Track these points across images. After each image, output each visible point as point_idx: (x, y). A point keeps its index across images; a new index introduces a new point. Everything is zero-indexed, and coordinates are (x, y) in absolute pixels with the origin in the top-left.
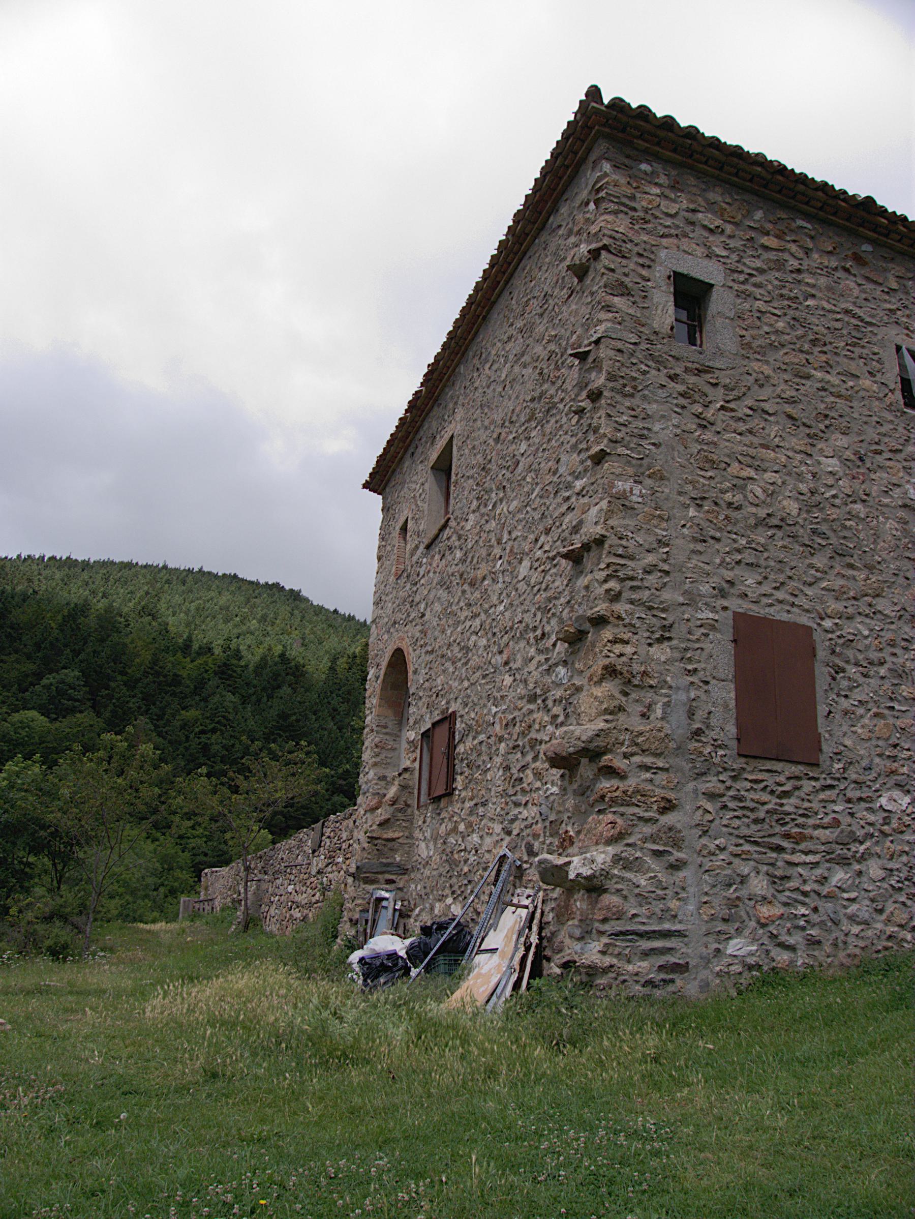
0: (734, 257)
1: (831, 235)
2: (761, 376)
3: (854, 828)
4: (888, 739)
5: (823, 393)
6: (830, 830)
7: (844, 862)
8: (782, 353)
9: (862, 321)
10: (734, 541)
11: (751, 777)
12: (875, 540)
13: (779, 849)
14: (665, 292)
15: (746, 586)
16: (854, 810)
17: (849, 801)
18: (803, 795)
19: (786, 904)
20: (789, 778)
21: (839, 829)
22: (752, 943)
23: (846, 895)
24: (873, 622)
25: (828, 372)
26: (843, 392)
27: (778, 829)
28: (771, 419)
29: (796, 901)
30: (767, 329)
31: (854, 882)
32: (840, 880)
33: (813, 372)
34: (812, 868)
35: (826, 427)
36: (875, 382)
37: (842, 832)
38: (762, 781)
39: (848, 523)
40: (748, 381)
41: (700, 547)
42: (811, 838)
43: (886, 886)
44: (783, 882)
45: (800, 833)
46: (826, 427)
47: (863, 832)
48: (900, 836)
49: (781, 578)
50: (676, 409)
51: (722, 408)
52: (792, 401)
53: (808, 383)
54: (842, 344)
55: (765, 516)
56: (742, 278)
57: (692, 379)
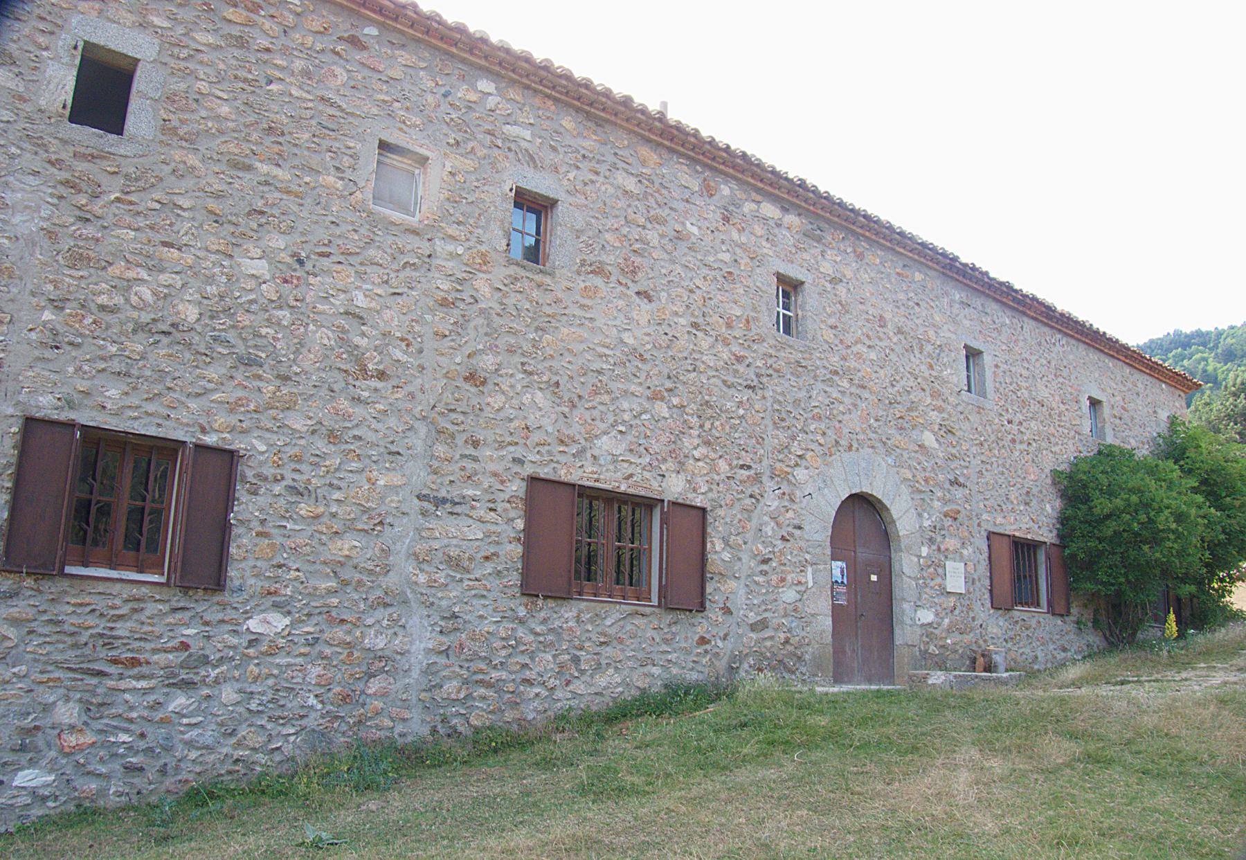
0: (180, 30)
1: (325, 13)
2: (182, 166)
3: (207, 652)
4: (271, 559)
5: (266, 189)
6: (175, 654)
7: (187, 685)
8: (218, 141)
9: (343, 110)
10: (101, 348)
11: (73, 601)
12: (297, 349)
13: (100, 674)
14: (67, 64)
15: (106, 397)
16: (211, 633)
17: (207, 623)
18: (143, 618)
19: (101, 732)
20: (127, 601)
21: (187, 653)
22: (50, 773)
23: (185, 721)
24: (275, 437)
25: (278, 165)
26: (294, 188)
27: (103, 653)
28: (186, 214)
29: (116, 727)
30: (204, 113)
31: (199, 706)
32: (180, 705)
33: (258, 165)
34: (144, 694)
35: (260, 225)
36: (342, 179)
37: (190, 655)
38: (89, 604)
39: (264, 331)
40: (162, 170)
41: (49, 354)
42: (148, 663)
43: (241, 709)
44: (101, 709)
45: (133, 658)
46: (260, 225)
47: (218, 655)
48: (270, 659)
49: (157, 389)
50: (50, 200)
51: (118, 200)
52: (218, 196)
53: (247, 176)
54: (306, 136)
55: (149, 321)
56: (184, 53)
57: (81, 166)
